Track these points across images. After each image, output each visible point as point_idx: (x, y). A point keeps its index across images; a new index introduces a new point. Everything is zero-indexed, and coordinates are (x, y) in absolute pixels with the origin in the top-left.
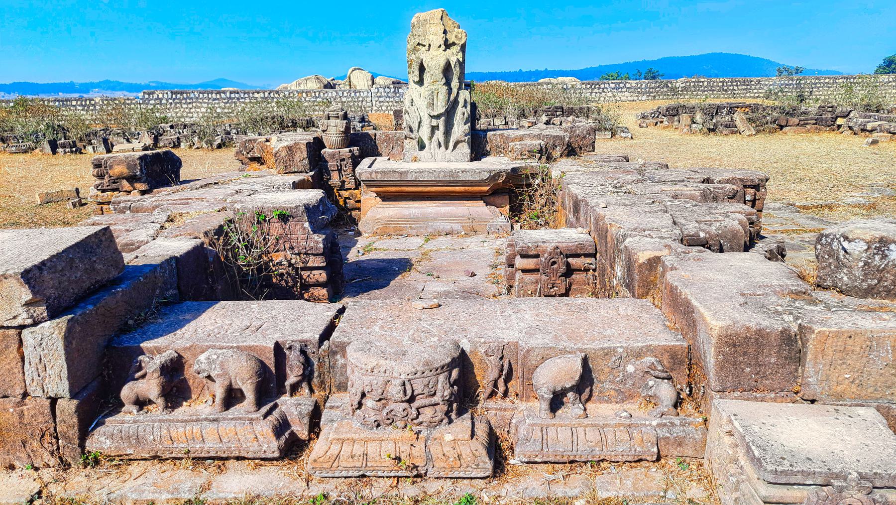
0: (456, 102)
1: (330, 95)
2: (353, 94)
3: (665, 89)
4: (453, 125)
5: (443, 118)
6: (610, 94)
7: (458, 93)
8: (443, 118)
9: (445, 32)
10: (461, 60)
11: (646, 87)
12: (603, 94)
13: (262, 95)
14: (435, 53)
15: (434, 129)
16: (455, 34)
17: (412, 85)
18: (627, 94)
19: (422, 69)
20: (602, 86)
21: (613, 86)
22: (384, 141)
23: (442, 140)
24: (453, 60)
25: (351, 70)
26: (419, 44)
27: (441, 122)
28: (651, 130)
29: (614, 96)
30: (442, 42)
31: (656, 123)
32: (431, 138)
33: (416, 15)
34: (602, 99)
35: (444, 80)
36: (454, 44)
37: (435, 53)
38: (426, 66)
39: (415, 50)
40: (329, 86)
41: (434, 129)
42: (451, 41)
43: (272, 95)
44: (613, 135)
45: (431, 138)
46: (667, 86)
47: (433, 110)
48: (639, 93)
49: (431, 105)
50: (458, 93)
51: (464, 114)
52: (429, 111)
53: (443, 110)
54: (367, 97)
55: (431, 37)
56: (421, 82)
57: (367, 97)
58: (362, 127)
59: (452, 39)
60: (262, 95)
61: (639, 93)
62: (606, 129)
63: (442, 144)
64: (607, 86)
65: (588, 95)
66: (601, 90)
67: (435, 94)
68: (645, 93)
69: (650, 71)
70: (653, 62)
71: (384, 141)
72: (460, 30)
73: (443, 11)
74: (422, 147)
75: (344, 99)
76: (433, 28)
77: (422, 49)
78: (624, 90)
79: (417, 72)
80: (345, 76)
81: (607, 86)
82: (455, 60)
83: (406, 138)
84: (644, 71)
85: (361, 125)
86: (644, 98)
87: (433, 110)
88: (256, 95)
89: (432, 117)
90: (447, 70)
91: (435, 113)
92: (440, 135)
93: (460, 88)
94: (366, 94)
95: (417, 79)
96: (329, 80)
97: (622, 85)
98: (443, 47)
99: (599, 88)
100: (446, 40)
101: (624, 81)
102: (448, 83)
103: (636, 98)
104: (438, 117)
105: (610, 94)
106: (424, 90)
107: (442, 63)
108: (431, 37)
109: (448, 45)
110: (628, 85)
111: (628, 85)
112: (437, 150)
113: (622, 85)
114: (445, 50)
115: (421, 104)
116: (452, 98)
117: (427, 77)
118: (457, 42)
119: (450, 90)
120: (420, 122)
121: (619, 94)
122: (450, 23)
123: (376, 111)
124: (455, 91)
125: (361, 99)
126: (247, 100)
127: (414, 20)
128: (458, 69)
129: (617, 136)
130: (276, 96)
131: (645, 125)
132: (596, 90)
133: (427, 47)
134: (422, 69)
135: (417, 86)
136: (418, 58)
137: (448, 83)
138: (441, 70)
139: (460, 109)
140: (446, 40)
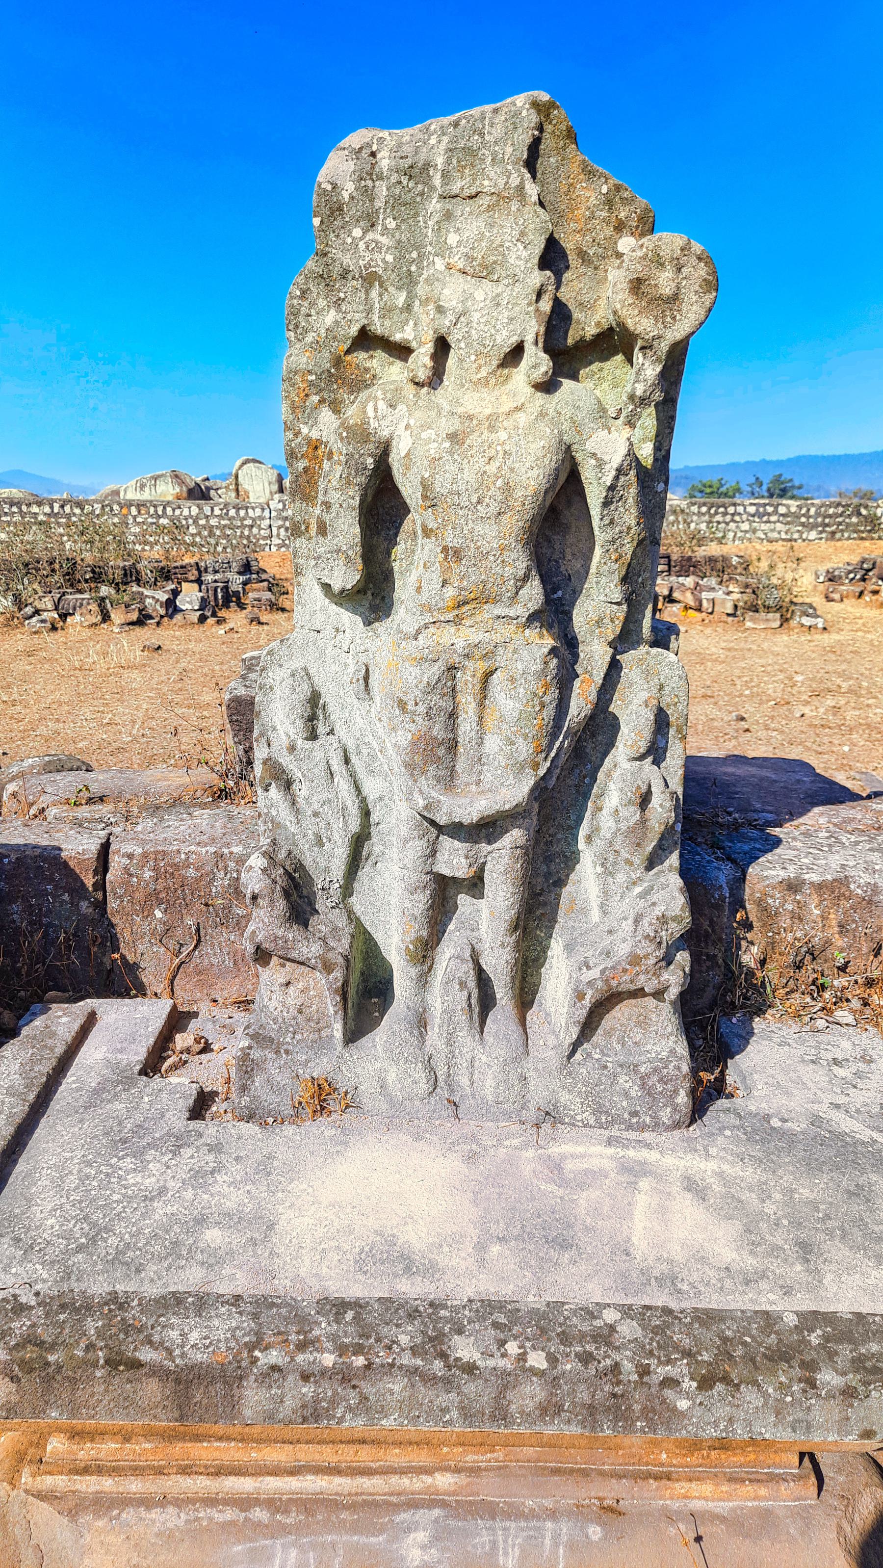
0: (601, 727)
1: (186, 512)
2: (232, 512)
3: (854, 520)
4: (571, 859)
5: (515, 836)
6: (745, 526)
7: (614, 666)
8: (515, 836)
9: (553, 257)
10: (646, 452)
11: (818, 514)
12: (732, 525)
13: (47, 509)
14: (478, 403)
15: (444, 896)
16: (616, 277)
17: (311, 604)
18: (779, 526)
19: (382, 508)
20: (731, 510)
21: (752, 510)
22: (154, 898)
23: (498, 962)
24: (610, 448)
25: (238, 463)
26: (365, 340)
27: (502, 858)
28: (851, 607)
29: (754, 531)
30: (531, 330)
31: (861, 594)
32: (425, 951)
33: (356, 139)
34: (731, 535)
35: (533, 594)
36: (615, 342)
37: (478, 403)
38: (409, 487)
39: (338, 379)
40: (199, 493)
41: (444, 896)
42: (587, 325)
43: (67, 509)
44: (785, 620)
45: (425, 951)
46: (859, 514)
47: (448, 781)
48: (803, 525)
49: (439, 752)
50: (614, 666)
51: (645, 800)
52: (428, 789)
53: (515, 791)
54: (261, 518)
55: (452, 292)
56: (372, 594)
57: (261, 518)
58: (245, 584)
59: (601, 299)
60: (47, 509)
61: (803, 525)
62: (768, 608)
63: (502, 992)
64: (740, 509)
65: (703, 526)
66: (728, 518)
67: (468, 680)
68: (814, 526)
69: (777, 479)
70: (779, 463)
71: (154, 898)
72: (669, 241)
73: (543, 110)
74: (366, 994)
75: (213, 522)
76: (469, 230)
77: (392, 372)
78: (773, 518)
79: (348, 530)
80: (230, 474)
81: (740, 509)
82: (616, 457)
83: (262, 956)
84: (767, 480)
85: (242, 578)
86: (813, 535)
87: (448, 781)
88: (35, 509)
89: (437, 829)
90: (557, 519)
91: (471, 808)
92: (486, 922)
93: (626, 639)
94: (258, 512)
95: (346, 577)
96: (199, 480)
97: (770, 509)
98: (536, 361)
99: (725, 514)
100: (559, 318)
101: (775, 501)
102: (555, 613)
103: (796, 536)
104: (487, 829)
105: (745, 526)
106: (398, 650)
107: (531, 476)
108: (452, 292)
109: (568, 351)
110: (782, 510)
111: (782, 510)
112: (465, 1038)
113: (770, 509)
114: (548, 386)
115: (376, 735)
116: (580, 703)
117: (415, 566)
118: (642, 324)
119: (568, 647)
120: (359, 844)
121: (764, 527)
122: (590, 194)
123: (280, 547)
124: (595, 653)
125: (248, 522)
126: (17, 518)
127: (337, 168)
128: (628, 515)
129: (793, 623)
130: (77, 511)
131: (837, 596)
132: (719, 518)
133: (423, 358)
134: (382, 508)
135: (348, 619)
136: (359, 434)
137: (555, 613)
138: (514, 523)
139: (620, 773)
140: (559, 318)
